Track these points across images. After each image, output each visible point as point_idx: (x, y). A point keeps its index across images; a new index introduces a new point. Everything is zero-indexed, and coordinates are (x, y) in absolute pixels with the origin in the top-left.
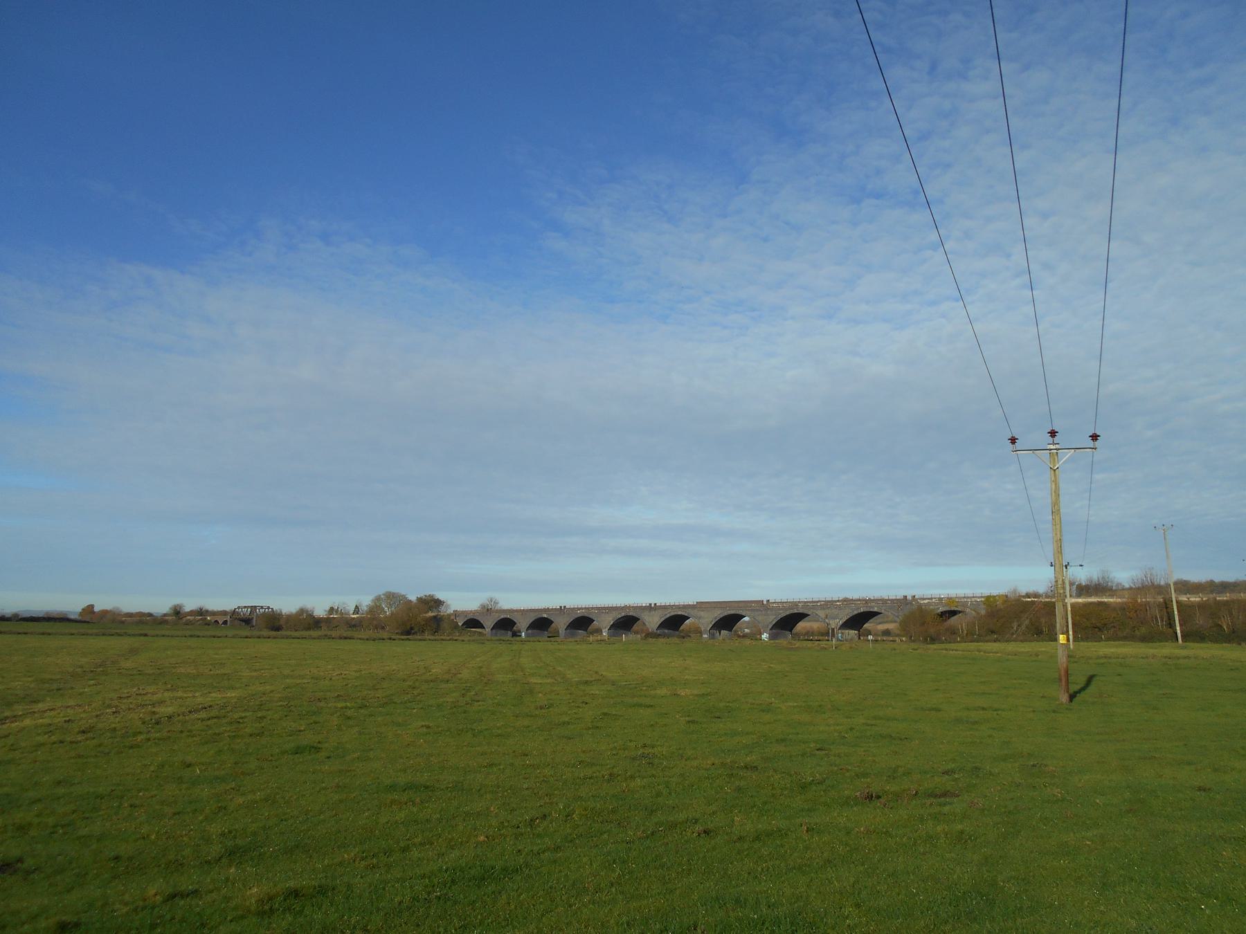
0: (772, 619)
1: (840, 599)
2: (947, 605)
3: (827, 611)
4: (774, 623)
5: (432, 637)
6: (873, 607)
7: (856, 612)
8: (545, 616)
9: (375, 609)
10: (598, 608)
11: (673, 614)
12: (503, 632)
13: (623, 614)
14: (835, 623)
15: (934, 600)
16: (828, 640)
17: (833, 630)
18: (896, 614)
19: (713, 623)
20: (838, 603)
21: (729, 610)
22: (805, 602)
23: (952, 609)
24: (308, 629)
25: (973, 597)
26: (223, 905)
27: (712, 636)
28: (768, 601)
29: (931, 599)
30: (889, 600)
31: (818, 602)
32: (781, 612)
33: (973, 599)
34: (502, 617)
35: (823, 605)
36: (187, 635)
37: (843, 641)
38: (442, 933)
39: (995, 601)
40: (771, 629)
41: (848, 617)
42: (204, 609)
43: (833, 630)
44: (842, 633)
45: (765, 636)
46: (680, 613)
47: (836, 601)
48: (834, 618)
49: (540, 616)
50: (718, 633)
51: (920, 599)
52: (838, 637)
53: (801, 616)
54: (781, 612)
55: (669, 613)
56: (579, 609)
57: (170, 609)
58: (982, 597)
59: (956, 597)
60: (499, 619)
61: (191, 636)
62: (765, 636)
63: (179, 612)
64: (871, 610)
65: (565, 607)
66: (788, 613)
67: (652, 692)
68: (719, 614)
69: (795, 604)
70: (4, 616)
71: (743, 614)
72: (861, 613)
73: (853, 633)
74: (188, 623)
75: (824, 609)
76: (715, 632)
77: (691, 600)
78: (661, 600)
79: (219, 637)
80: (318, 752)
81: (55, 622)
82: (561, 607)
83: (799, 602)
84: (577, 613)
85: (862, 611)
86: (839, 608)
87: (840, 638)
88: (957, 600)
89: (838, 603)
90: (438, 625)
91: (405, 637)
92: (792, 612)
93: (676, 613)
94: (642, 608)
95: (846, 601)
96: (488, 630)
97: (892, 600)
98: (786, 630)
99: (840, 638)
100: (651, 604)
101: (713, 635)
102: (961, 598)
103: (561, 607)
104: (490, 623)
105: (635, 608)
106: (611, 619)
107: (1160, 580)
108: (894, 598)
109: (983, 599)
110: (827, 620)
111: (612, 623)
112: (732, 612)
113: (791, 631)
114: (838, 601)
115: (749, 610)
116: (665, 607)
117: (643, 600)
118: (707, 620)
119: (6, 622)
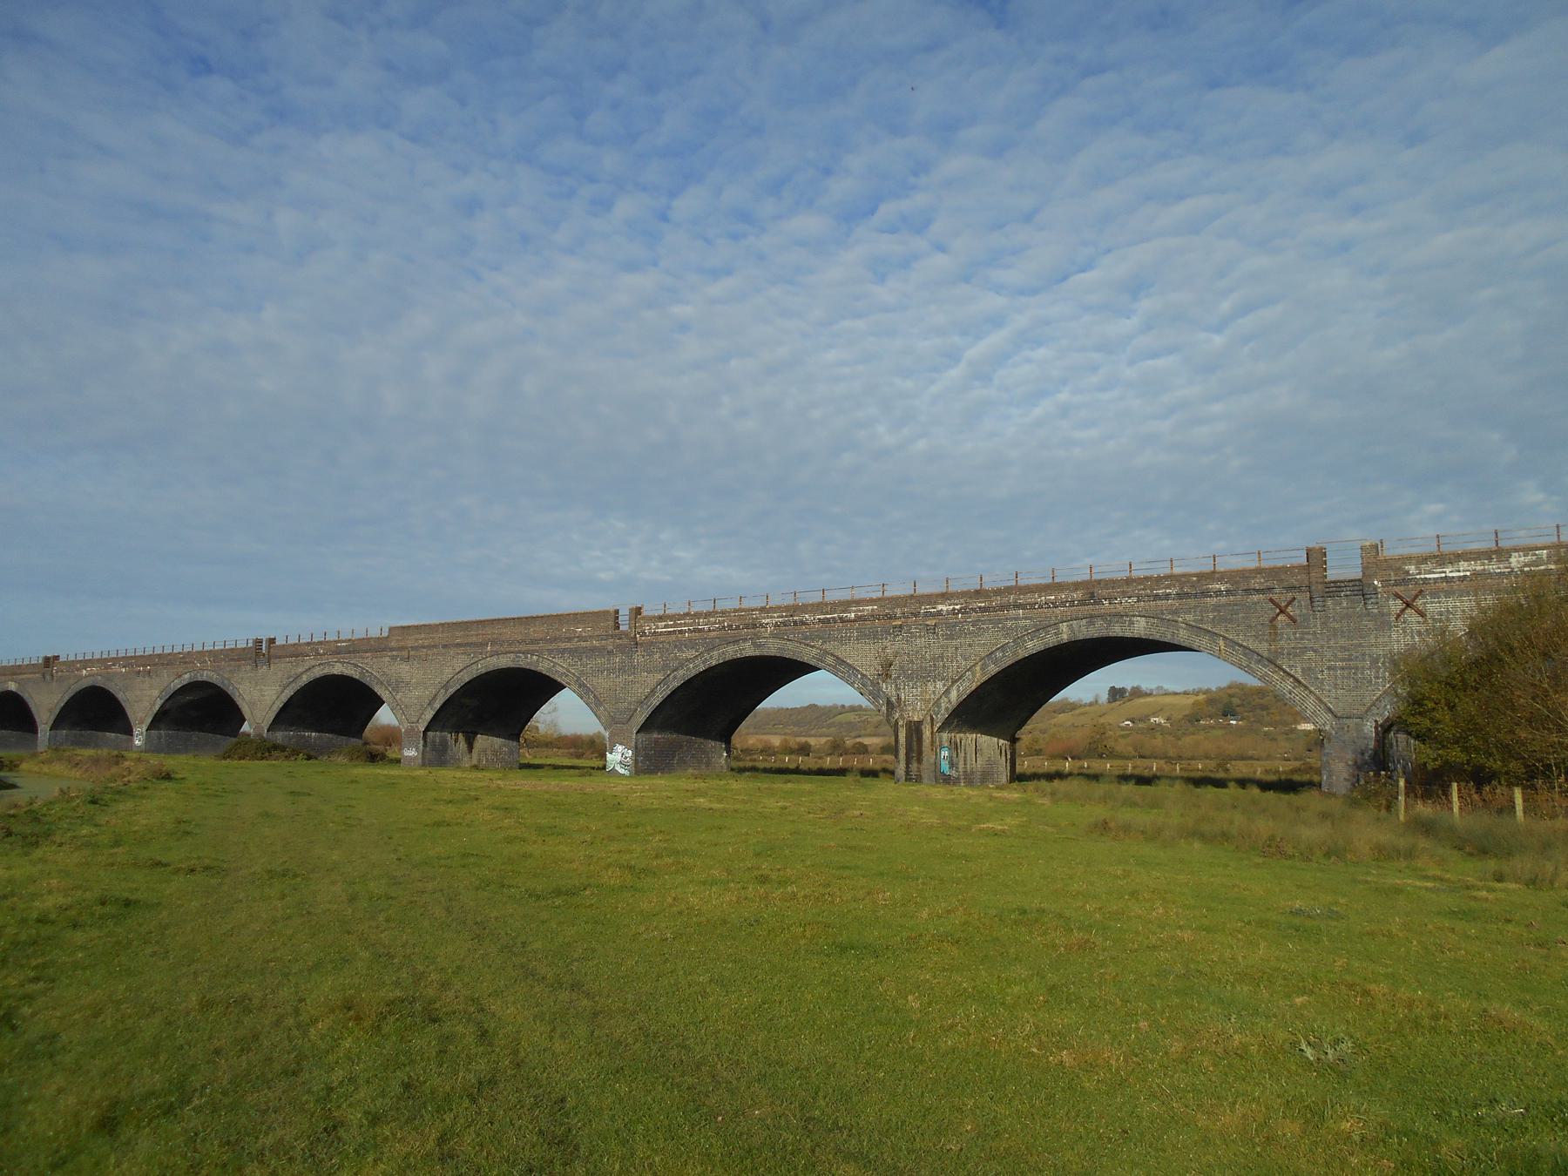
3: (891, 646)
4: (656, 701)
7: (1033, 646)
10: (128, 661)
11: (318, 672)
13: (186, 679)
17: (915, 729)
18: (1263, 648)
19: (437, 705)
22: (794, 609)
26: (98, 1092)
27: (437, 756)
28: (638, 611)
30: (1212, 576)
31: (846, 605)
32: (691, 654)
35: (873, 616)
37: (956, 781)
39: (93, 756)
40: (644, 728)
41: (993, 669)
43: (915, 729)
44: (955, 747)
45: (619, 757)
46: (338, 669)
47: (932, 599)
50: (462, 744)
51: (1423, 560)
52: (937, 765)
54: (691, 654)
56: (86, 663)
65: (272, 641)
66: (715, 658)
67: (186, 952)
68: (457, 669)
69: (748, 622)
71: (807, 655)
73: (990, 745)
75: (875, 636)
77: (375, 625)
78: (287, 627)
83: (762, 610)
84: (81, 678)
85: (1065, 637)
87: (945, 767)
92: (731, 652)
93: (327, 671)
94: (235, 656)
98: (707, 735)
99: (945, 767)
100: (258, 642)
105: (356, 647)
106: (156, 693)
107: (456, 741)
108: (1250, 563)
110: (888, 688)
111: (157, 707)
112: (504, 662)
113: (726, 736)
114: (945, 597)
115: (563, 651)
116: (296, 652)
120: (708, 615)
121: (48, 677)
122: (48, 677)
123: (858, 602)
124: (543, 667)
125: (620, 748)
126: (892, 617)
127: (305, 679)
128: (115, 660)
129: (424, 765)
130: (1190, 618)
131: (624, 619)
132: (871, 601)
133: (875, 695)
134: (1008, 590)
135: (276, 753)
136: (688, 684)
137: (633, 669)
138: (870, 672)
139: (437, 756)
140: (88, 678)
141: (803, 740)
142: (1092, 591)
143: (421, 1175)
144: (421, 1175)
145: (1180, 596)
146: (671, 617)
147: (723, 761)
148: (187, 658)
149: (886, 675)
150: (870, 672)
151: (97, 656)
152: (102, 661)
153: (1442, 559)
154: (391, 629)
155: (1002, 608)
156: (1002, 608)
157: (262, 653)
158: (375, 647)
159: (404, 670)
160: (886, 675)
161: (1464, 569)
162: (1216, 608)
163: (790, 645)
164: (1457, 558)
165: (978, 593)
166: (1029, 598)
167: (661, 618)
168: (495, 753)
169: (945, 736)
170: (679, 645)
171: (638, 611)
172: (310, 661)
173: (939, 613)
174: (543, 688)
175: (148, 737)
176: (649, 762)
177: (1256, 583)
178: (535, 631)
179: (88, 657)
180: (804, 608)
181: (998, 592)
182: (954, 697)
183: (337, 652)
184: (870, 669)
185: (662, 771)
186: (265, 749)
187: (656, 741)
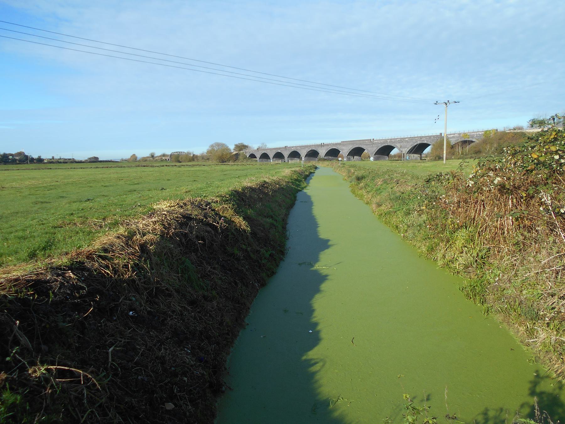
0: (375, 149)
1: (484, 130)
2: (463, 137)
3: (402, 144)
5: (233, 163)
6: (423, 141)
8: (279, 151)
9: (209, 152)
10: (300, 147)
11: (331, 148)
12: (266, 160)
13: (310, 149)
14: (405, 150)
15: (456, 135)
16: (401, 160)
20: (407, 139)
21: (356, 145)
22: (391, 139)
23: (466, 140)
24: (190, 161)
25: (478, 132)
28: (373, 139)
29: (455, 134)
31: (397, 139)
32: (380, 145)
33: (478, 133)
34: (263, 152)
35: (400, 140)
36: (70, 168)
38: (1, 197)
42: (229, 147)
43: (404, 154)
45: (372, 159)
48: (405, 148)
49: (277, 152)
51: (449, 135)
52: (406, 158)
53: (425, 146)
54: (380, 145)
55: (330, 147)
56: (293, 147)
57: (150, 155)
58: (482, 131)
59: (469, 133)
60: (262, 153)
61: (103, 168)
62: (372, 159)
63: (153, 156)
64: (423, 142)
65: (287, 146)
68: (351, 147)
69: (386, 141)
70: (111, 160)
72: (425, 143)
73: (416, 156)
74: (157, 160)
76: (350, 157)
77: (339, 141)
78: (326, 142)
79: (84, 168)
80: (106, 250)
81: (104, 162)
82: (285, 147)
86: (407, 142)
88: (469, 134)
89: (407, 139)
90: (238, 158)
91: (222, 163)
94: (318, 146)
95: (412, 139)
96: (258, 159)
97: (434, 136)
101: (350, 158)
102: (471, 133)
103: (285, 147)
104: (259, 155)
105: (336, 144)
106: (305, 152)
109: (483, 133)
110: (401, 149)
111: (306, 154)
112: (357, 146)
115: (364, 145)
116: (328, 145)
117: (319, 142)
118: (345, 151)
119: (83, 163)
120: (382, 140)
121: (286, 150)
122: (286, 150)
123: (398, 138)
124: (393, 145)
125: (372, 157)
126: (401, 140)
127: (329, 149)
128: (298, 146)
129: (347, 161)
130: (430, 141)
131: (372, 140)
132: (399, 138)
133: (400, 150)
134: (413, 137)
135: (326, 160)
136: (380, 149)
137: (373, 147)
138: (399, 147)
139: (349, 159)
140: (293, 149)
141: (97, 166)
142: (421, 137)
143: (564, 291)
144: (564, 291)
145: (429, 138)
146: (378, 140)
147: (387, 159)
148: (310, 146)
149: (401, 148)
150: (399, 147)
151: (294, 146)
152: (295, 147)
153: (451, 134)
154: (341, 142)
155: (413, 139)
156: (413, 139)
157: (322, 145)
158: (339, 144)
159: (344, 148)
160: (401, 148)
161: (452, 136)
162: (432, 140)
163: (391, 144)
164: (452, 134)
165: (410, 138)
166: (415, 138)
167: (376, 140)
168: (357, 159)
169: (408, 155)
170: (379, 144)
171: (373, 139)
172: (330, 146)
173: (406, 140)
174: (392, 148)
175: (305, 159)
176: (376, 159)
177: (435, 137)
178: (361, 142)
179: (293, 146)
180: (392, 139)
181: (412, 137)
182: (408, 150)
183: (334, 145)
184: (399, 147)
185: (378, 160)
186: (324, 160)
187: (377, 156)
